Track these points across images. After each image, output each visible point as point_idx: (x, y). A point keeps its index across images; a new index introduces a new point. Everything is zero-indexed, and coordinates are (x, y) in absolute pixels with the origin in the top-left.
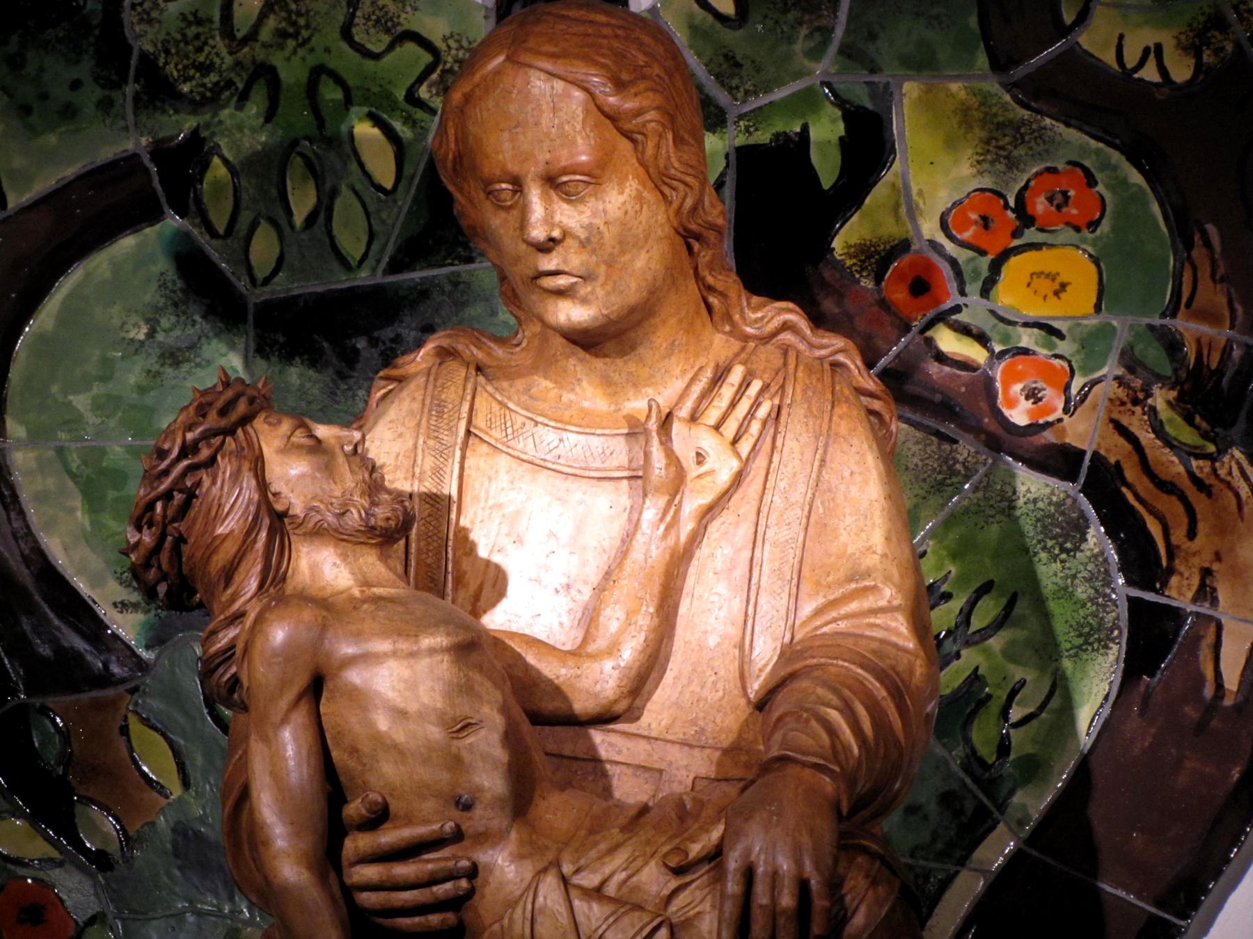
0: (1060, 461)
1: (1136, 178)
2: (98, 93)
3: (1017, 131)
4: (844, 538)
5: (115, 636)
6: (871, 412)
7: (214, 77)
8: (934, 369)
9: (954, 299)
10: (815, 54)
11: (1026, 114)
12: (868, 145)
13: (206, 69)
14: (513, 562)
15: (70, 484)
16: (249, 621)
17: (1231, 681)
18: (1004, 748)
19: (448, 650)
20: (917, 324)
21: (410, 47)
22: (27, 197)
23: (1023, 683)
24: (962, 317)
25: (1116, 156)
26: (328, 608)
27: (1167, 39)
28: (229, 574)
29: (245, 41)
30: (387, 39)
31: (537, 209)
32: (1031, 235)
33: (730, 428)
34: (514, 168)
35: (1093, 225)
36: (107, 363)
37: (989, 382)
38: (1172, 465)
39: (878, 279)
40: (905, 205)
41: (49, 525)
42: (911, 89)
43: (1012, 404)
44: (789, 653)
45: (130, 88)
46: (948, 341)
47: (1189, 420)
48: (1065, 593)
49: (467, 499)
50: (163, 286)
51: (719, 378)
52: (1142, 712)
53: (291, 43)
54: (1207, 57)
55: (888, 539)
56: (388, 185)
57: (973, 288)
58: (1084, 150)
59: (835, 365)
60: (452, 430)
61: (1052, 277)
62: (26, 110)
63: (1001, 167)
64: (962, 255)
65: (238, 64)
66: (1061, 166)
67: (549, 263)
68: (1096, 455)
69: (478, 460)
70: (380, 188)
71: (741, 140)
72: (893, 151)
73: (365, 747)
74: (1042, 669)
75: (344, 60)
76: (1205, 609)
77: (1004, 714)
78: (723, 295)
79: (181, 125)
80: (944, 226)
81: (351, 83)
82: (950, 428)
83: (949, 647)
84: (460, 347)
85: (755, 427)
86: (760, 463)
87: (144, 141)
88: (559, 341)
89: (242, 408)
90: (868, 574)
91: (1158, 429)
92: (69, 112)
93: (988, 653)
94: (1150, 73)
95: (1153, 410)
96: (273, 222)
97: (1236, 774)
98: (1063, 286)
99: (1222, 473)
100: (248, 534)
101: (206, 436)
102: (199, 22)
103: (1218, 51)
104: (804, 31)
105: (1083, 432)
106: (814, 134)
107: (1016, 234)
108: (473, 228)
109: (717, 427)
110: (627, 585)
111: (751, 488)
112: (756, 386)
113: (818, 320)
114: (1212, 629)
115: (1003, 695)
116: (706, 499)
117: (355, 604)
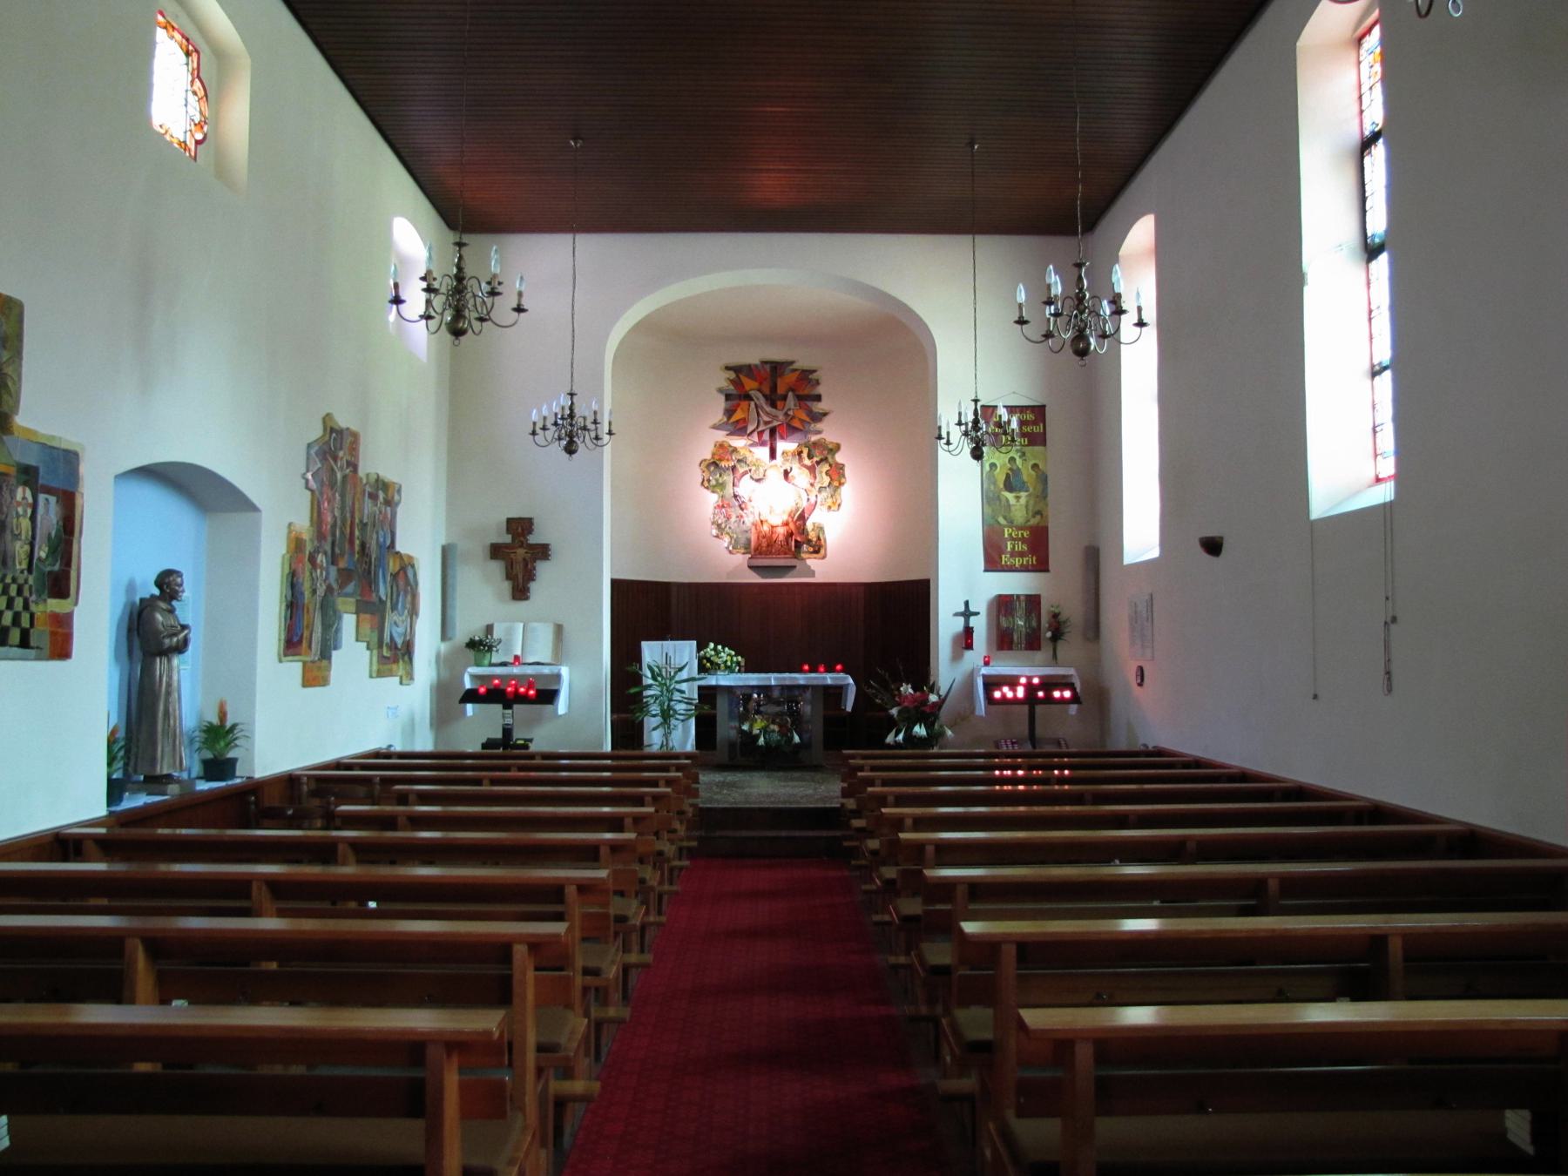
17: (849, 709)
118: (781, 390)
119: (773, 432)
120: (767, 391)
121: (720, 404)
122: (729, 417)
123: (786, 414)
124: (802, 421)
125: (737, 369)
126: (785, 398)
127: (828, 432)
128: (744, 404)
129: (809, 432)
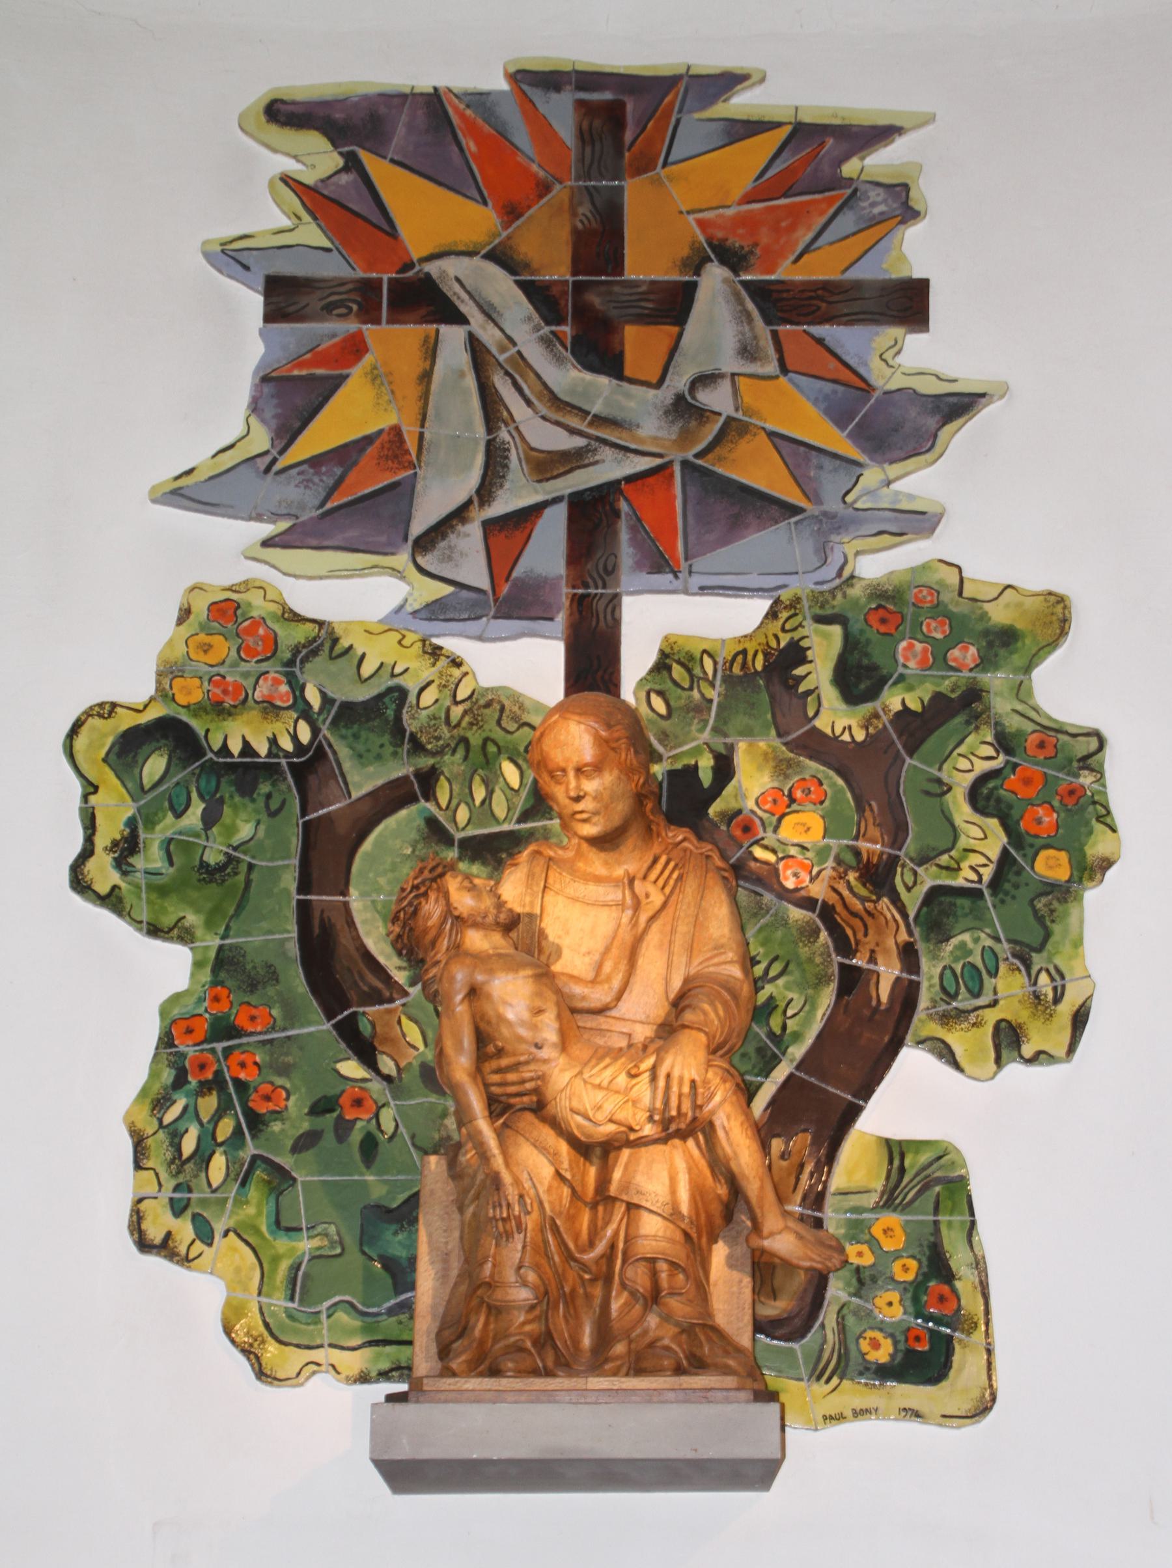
0: (808, 903)
1: (840, 782)
2: (391, 749)
3: (789, 763)
4: (712, 930)
5: (396, 982)
6: (724, 878)
7: (441, 742)
8: (753, 864)
9: (761, 834)
10: (701, 730)
11: (792, 755)
12: (724, 769)
13: (438, 738)
14: (565, 943)
15: (377, 916)
16: (442, 965)
17: (884, 996)
18: (784, 1027)
19: (531, 976)
20: (746, 845)
21: (526, 729)
22: (364, 791)
23: (792, 1000)
24: (765, 842)
25: (831, 773)
26: (480, 959)
27: (854, 723)
28: (433, 943)
29: (455, 727)
30: (516, 726)
31: (573, 784)
32: (795, 807)
33: (661, 882)
34: (562, 764)
35: (822, 803)
36: (394, 864)
37: (776, 870)
38: (857, 905)
39: (729, 825)
40: (740, 794)
41: (368, 933)
42: (742, 746)
43: (786, 879)
44: (687, 981)
45: (406, 746)
46: (758, 852)
47: (864, 885)
48: (810, 960)
49: (545, 915)
50: (419, 831)
51: (655, 861)
52: (845, 1012)
53: (475, 728)
54: (871, 730)
55: (731, 931)
56: (516, 787)
57: (770, 829)
58: (818, 770)
59: (708, 857)
60: (538, 884)
61: (804, 825)
62: (360, 756)
63: (781, 778)
64: (765, 816)
65: (452, 737)
66: (807, 777)
67: (580, 806)
68: (824, 902)
69: (550, 898)
70: (512, 789)
71: (669, 768)
72: (734, 773)
73: (494, 1021)
74: (801, 993)
75: (498, 734)
76: (871, 967)
77: (785, 1012)
78: (658, 824)
79: (425, 762)
80: (757, 803)
81: (501, 744)
82: (759, 890)
83: (760, 984)
84: (542, 849)
85: (672, 882)
86: (674, 898)
87: (411, 769)
88: (585, 846)
89: (440, 870)
90: (722, 946)
91: (850, 888)
92: (379, 757)
93: (777, 986)
94: (846, 737)
95: (848, 882)
96: (467, 804)
97: (886, 1039)
98: (809, 829)
99: (879, 908)
100: (442, 924)
101: (423, 882)
102: (435, 718)
103: (876, 728)
104: (696, 721)
105: (818, 891)
106: (700, 764)
107: (789, 806)
108: (547, 794)
109: (655, 882)
110: (615, 951)
111: (670, 910)
112: (672, 864)
113: (700, 838)
114: (875, 977)
115: (783, 1005)
116: (650, 913)
117: (490, 957)
118: (646, 261)
119: (592, 516)
120: (557, 270)
121: (240, 336)
122: (288, 432)
123: (684, 409)
124: (796, 452)
125: (351, 123)
126: (674, 304)
127: (1015, 1001)
128: (393, 341)
129: (831, 526)
